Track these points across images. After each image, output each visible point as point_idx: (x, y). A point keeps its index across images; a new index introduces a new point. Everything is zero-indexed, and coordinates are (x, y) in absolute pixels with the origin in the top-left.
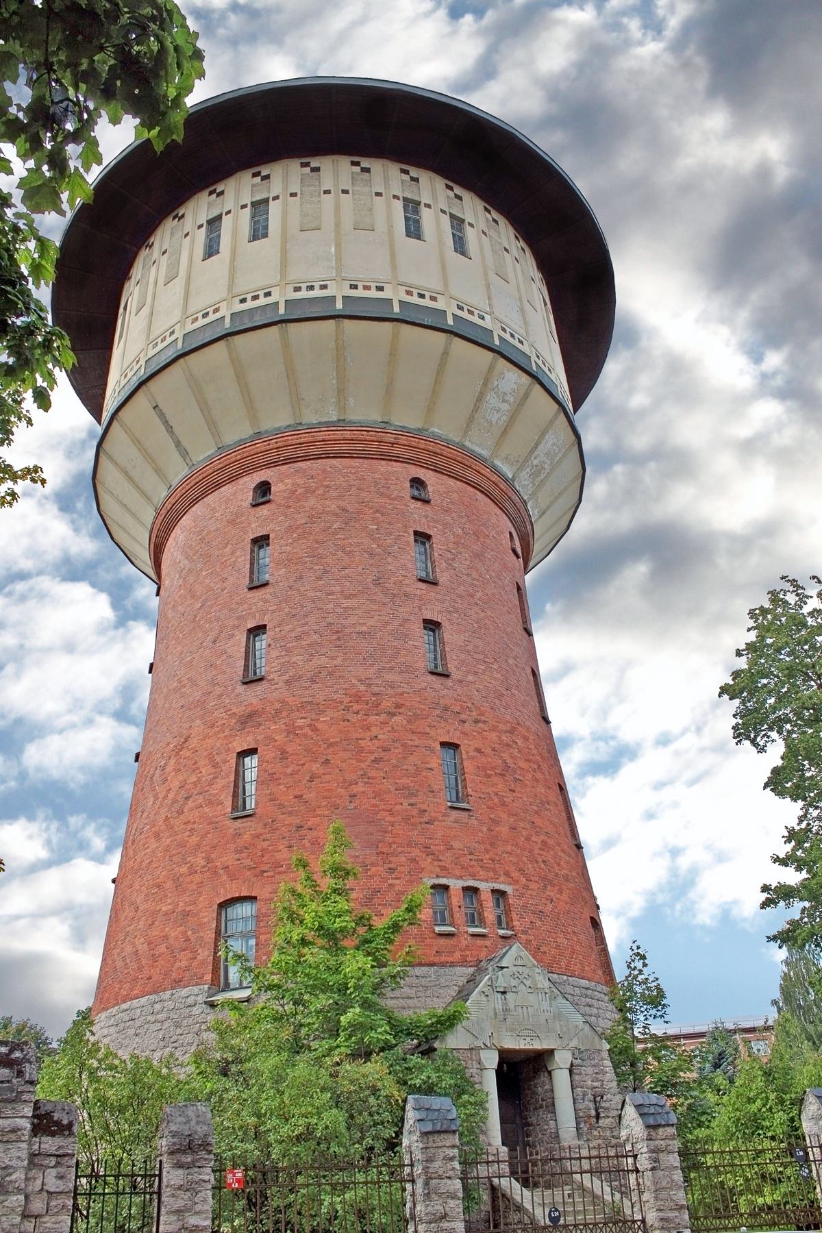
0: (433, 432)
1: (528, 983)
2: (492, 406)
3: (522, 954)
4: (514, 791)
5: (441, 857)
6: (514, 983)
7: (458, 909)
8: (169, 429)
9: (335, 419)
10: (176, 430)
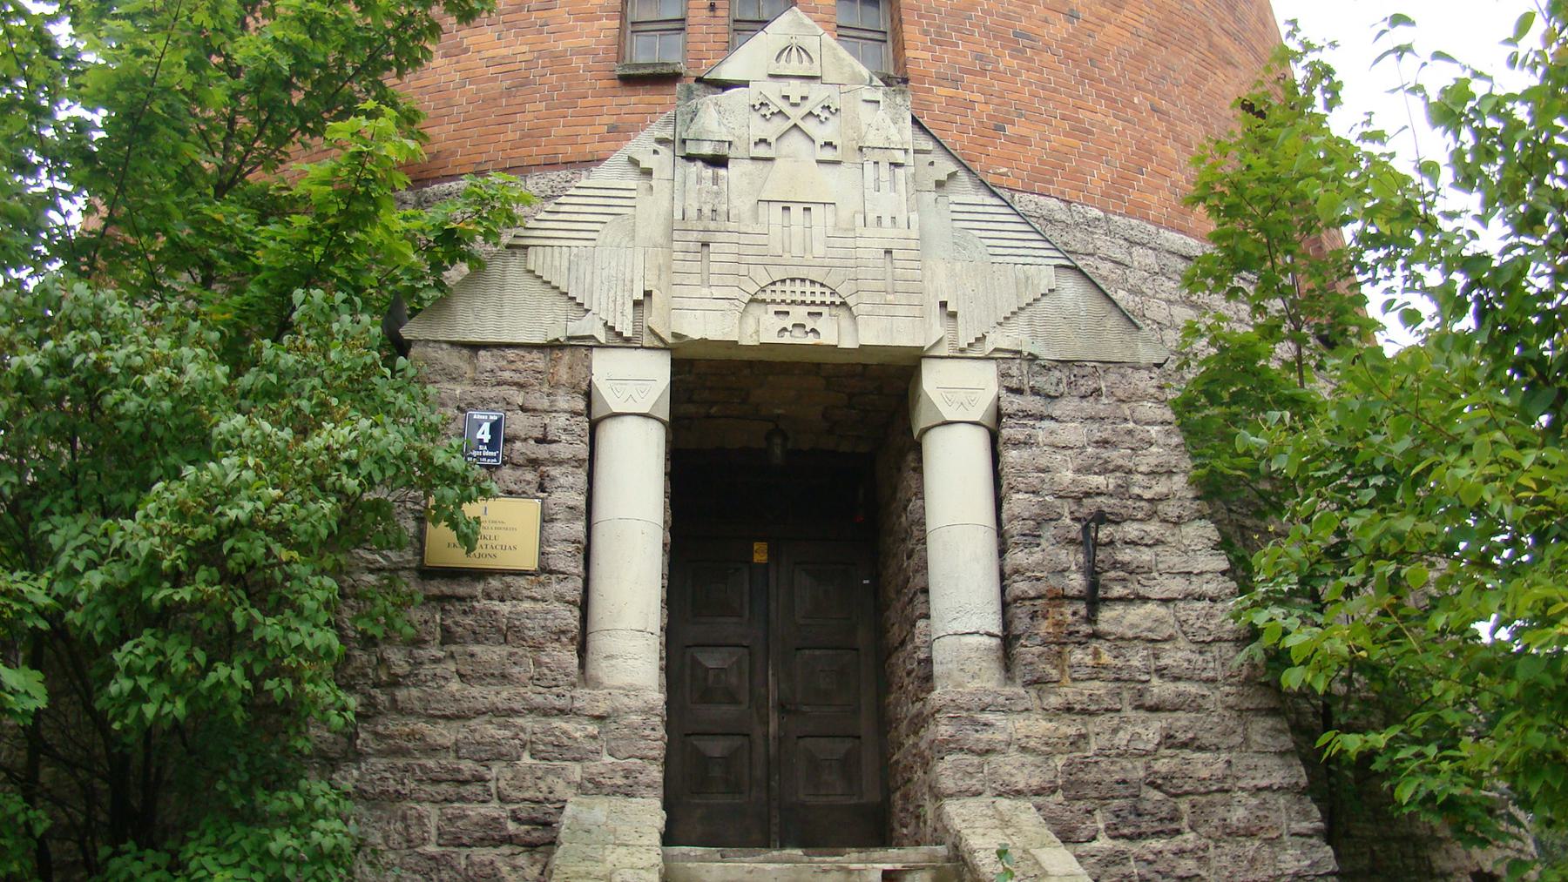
1: (821, 133)
3: (811, 44)
6: (759, 128)
7: (706, 13)
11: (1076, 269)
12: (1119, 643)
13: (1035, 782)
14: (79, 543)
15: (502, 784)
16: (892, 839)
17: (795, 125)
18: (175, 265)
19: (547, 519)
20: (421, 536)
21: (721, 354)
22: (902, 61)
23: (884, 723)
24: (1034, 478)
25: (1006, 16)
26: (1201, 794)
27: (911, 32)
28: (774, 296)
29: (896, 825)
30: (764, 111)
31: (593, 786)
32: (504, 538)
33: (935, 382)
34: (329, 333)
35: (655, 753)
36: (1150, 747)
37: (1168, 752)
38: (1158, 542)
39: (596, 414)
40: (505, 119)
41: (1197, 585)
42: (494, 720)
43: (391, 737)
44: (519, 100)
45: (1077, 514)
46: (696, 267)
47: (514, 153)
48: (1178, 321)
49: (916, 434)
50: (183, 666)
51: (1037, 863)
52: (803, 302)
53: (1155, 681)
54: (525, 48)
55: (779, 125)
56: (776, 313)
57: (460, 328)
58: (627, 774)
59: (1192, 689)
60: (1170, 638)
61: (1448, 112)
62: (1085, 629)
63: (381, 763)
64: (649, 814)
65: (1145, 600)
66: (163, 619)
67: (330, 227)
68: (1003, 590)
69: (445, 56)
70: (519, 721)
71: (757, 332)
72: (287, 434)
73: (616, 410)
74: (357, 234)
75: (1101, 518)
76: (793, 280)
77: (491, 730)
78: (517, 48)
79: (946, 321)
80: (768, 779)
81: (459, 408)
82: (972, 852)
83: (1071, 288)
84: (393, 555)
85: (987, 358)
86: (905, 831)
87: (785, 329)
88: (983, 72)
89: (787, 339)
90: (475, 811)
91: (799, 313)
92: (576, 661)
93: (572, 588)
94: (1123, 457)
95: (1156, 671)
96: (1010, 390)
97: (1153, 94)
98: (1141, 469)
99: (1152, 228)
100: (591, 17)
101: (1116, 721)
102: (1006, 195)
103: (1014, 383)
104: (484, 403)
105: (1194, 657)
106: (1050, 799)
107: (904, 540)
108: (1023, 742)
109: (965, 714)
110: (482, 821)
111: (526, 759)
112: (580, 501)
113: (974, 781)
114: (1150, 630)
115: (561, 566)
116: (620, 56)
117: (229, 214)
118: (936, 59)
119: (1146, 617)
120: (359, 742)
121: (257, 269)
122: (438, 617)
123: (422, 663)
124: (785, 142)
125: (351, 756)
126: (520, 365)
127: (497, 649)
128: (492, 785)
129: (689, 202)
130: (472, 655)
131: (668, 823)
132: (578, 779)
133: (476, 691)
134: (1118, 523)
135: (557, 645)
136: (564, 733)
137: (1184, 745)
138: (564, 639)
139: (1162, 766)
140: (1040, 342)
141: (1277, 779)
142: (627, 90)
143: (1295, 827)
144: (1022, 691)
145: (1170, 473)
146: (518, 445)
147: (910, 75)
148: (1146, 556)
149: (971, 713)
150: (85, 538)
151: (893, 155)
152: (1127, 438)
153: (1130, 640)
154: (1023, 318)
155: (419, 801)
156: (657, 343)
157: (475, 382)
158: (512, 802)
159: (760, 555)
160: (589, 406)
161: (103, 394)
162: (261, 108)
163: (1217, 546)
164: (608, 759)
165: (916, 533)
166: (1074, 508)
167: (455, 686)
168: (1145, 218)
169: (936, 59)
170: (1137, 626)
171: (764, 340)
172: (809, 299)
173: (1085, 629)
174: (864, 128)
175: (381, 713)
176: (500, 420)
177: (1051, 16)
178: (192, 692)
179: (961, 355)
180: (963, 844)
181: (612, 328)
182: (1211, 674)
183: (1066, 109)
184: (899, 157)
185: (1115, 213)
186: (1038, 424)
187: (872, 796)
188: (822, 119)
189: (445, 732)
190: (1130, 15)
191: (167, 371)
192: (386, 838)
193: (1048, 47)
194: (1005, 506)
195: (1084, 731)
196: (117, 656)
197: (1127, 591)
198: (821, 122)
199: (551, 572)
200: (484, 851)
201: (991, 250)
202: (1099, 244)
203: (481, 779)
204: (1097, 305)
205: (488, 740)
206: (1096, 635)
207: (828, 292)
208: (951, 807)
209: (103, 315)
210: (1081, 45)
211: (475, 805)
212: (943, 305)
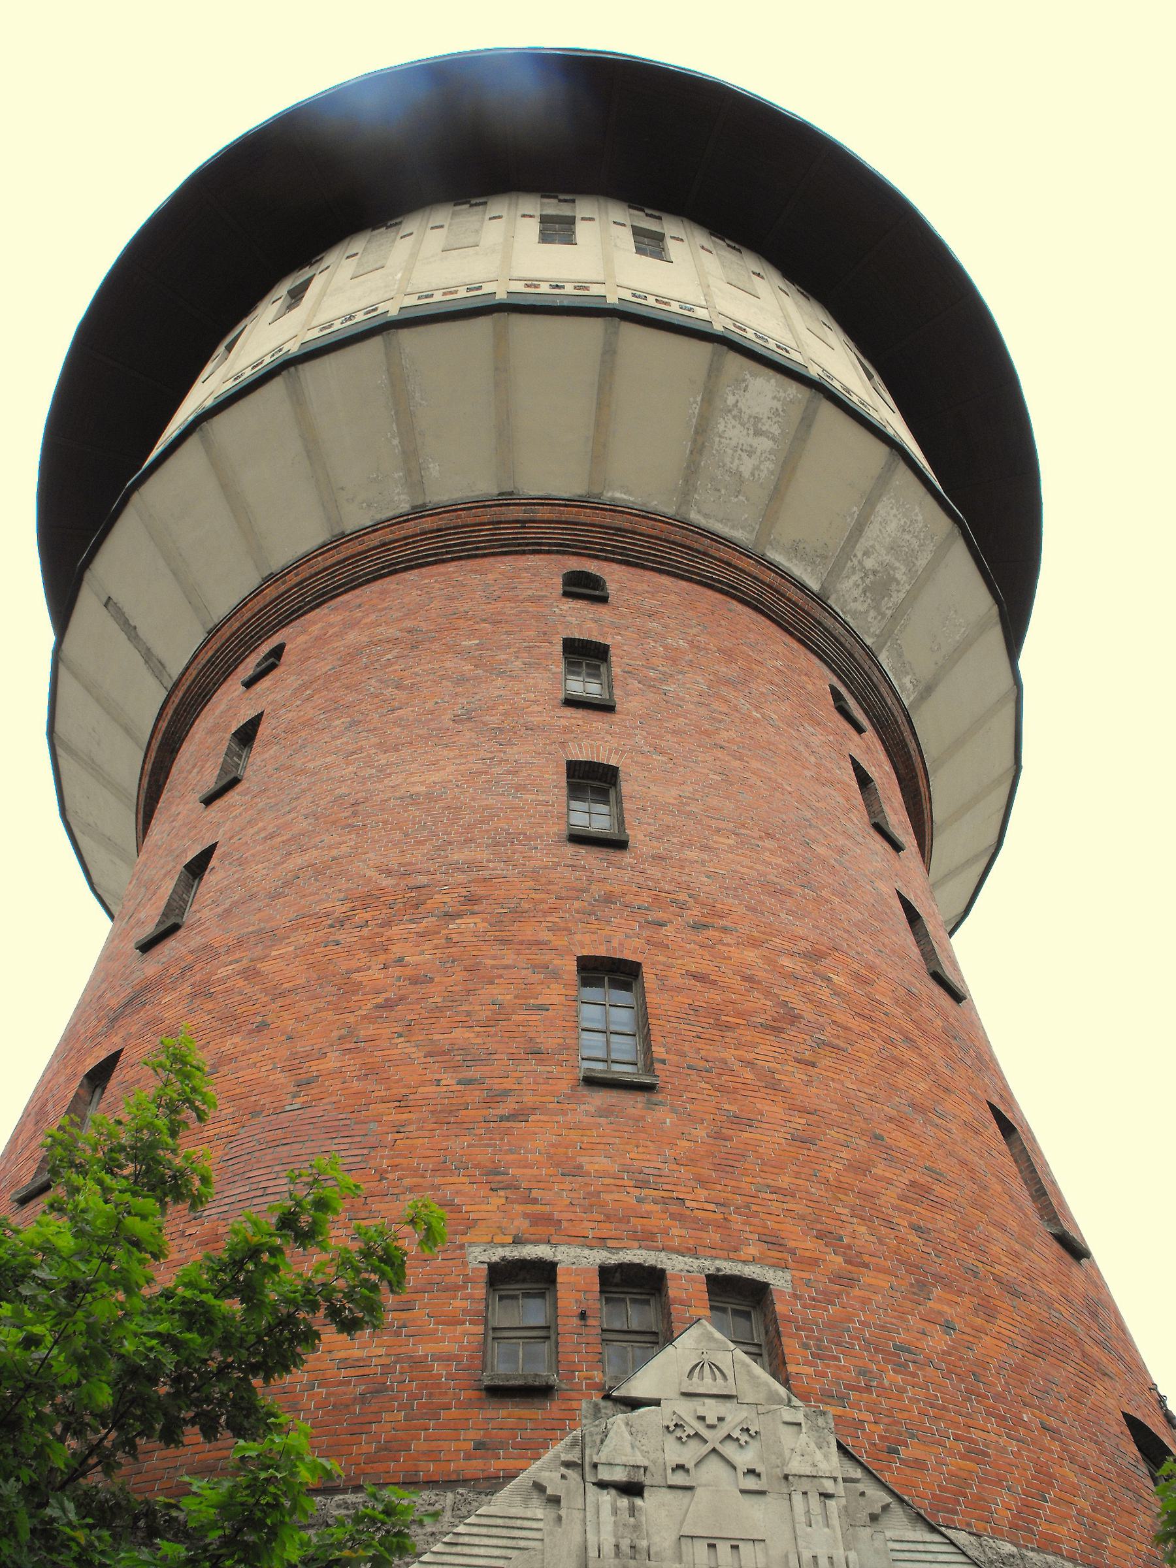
0: (613, 499)
1: (744, 1458)
2: (734, 443)
3: (723, 1360)
4: (814, 1065)
5: (535, 1194)
6: (674, 1453)
7: (575, 1321)
8: (130, 631)
9: (405, 507)
10: (143, 631)
17: (714, 1450)
25: (883, 1328)
27: (790, 1345)
30: (679, 1433)
54: (382, 1351)
61: (384, 1249)
88: (868, 1388)
100: (454, 1321)
118: (821, 1375)
129: (604, 1536)
151: (822, 1485)
168: (1058, 1553)
169: (821, 1375)
174: (787, 1453)
177: (929, 1327)
183: (958, 1428)
184: (829, 1487)
188: (742, 1442)
190: (1003, 1325)
198: (741, 1446)
210: (961, 1358)
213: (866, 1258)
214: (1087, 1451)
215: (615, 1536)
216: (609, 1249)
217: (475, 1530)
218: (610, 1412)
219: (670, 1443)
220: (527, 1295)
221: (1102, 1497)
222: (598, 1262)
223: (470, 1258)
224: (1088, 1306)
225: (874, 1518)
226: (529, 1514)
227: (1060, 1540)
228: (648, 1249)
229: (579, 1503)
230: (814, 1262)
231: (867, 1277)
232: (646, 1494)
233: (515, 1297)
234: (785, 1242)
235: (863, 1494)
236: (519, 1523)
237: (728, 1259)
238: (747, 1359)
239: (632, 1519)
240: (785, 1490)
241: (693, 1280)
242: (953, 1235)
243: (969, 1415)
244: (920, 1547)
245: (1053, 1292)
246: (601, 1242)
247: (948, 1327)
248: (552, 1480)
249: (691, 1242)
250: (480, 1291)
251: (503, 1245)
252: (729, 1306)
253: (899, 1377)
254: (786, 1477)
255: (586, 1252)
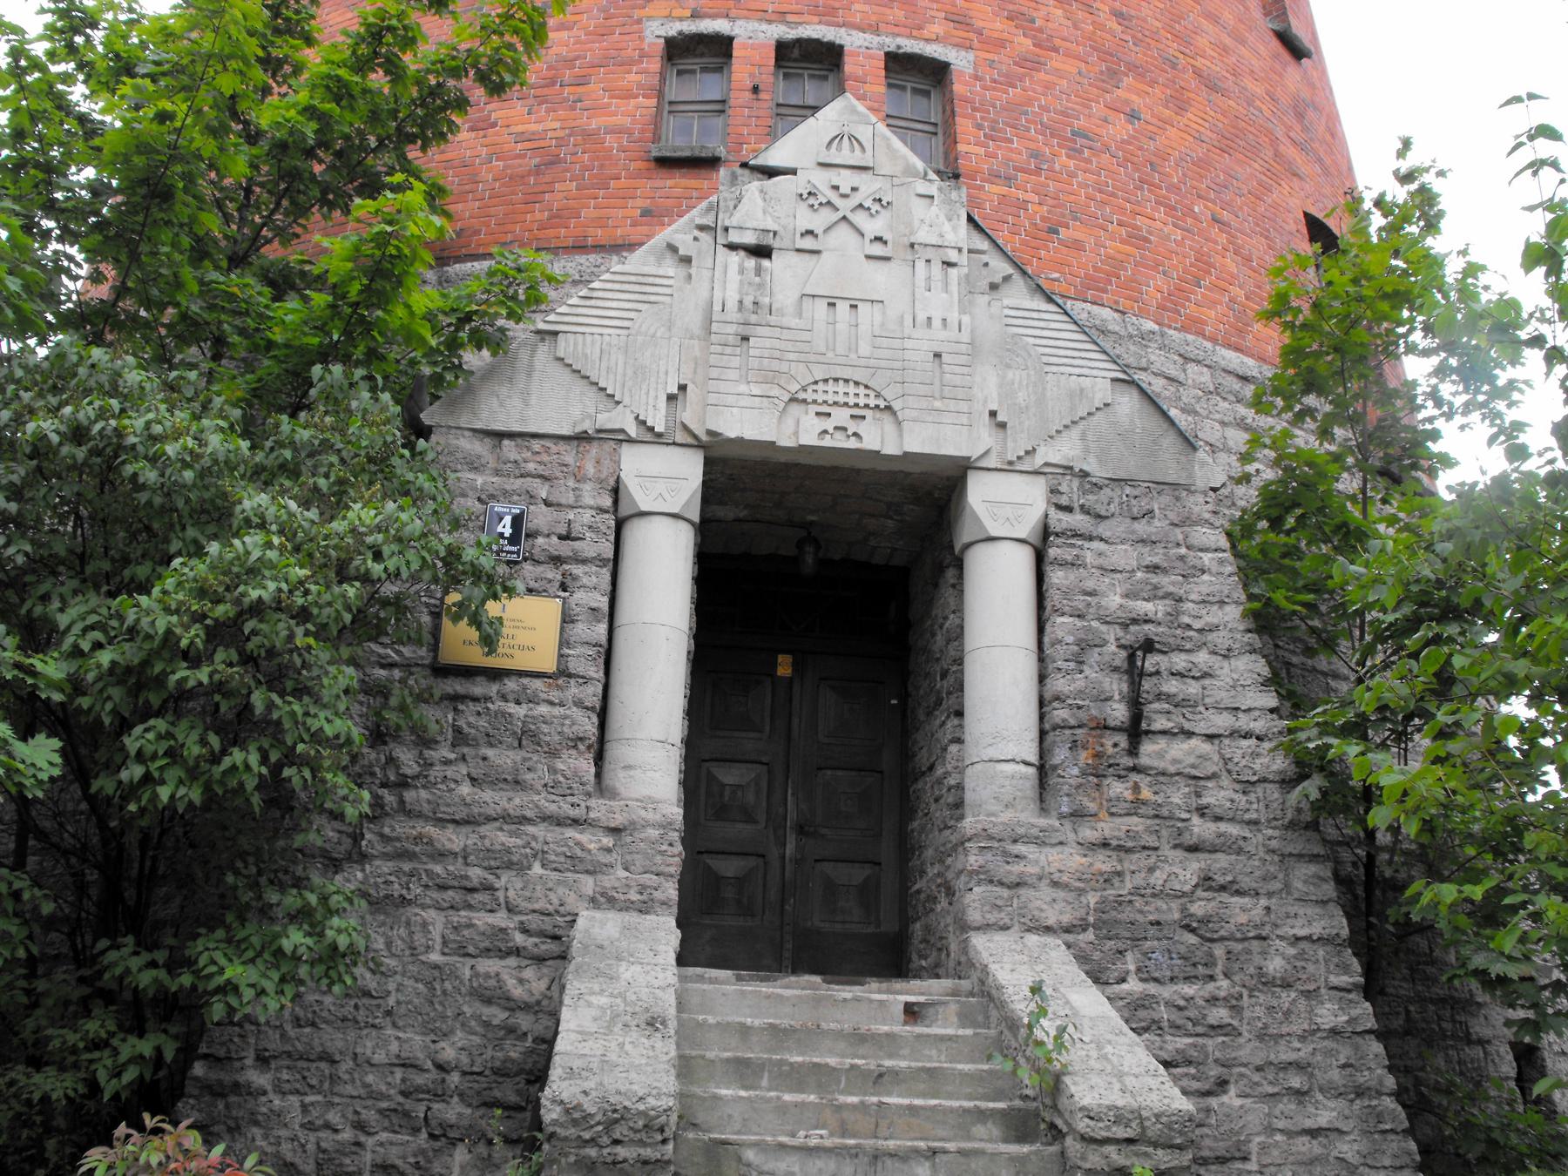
1: (872, 227)
3: (864, 133)
6: (806, 219)
7: (748, 95)
11: (1132, 383)
12: (1161, 779)
13: (1066, 919)
14: (88, 622)
15: (511, 893)
16: (908, 970)
17: (844, 218)
18: (183, 340)
19: (567, 619)
20: (436, 632)
21: (755, 454)
22: (952, 157)
23: (906, 849)
24: (1079, 601)
26: (1237, 940)
27: (963, 125)
28: (815, 396)
29: (914, 957)
30: (811, 201)
31: (605, 900)
32: (523, 638)
33: (981, 494)
34: (349, 412)
35: (672, 870)
36: (1187, 888)
37: (1206, 894)
38: (1206, 675)
39: (624, 511)
40: (533, 199)
41: (1244, 723)
42: (506, 827)
43: (398, 839)
44: (547, 179)
45: (1123, 641)
46: (736, 361)
47: (541, 234)
48: (1231, 443)
49: (957, 550)
50: (196, 750)
51: (1067, 1002)
52: (846, 404)
53: (1196, 820)
54: (557, 125)
55: (827, 216)
56: (818, 414)
57: (484, 415)
58: (642, 889)
59: (1233, 830)
60: (1214, 776)
62: (1128, 761)
63: (386, 867)
64: (665, 933)
65: (1190, 734)
66: (177, 703)
67: (351, 305)
68: (1042, 717)
69: (472, 129)
70: (531, 829)
71: (796, 433)
72: (313, 514)
73: (644, 508)
74: (380, 313)
75: (1148, 646)
76: (836, 380)
77: (502, 837)
78: (548, 124)
79: (994, 430)
80: (783, 902)
81: (479, 499)
82: (999, 988)
83: (1128, 403)
84: (407, 651)
85: (1036, 473)
86: (924, 963)
87: (825, 432)
89: (827, 442)
90: (482, 920)
91: (841, 416)
92: (593, 770)
93: (592, 693)
94: (1173, 584)
95: (1197, 809)
96: (1059, 507)
97: (1214, 202)
98: (1193, 597)
99: (1208, 345)
101: (1153, 860)
102: (1060, 301)
103: (1064, 501)
104: (506, 495)
105: (1236, 797)
106: (1081, 937)
107: (938, 660)
108: (1056, 877)
109: (996, 844)
110: (489, 932)
111: (537, 869)
112: (602, 603)
113: (1003, 915)
114: (1193, 766)
115: (581, 670)
116: (656, 139)
117: (247, 286)
119: (1190, 752)
120: (364, 843)
121: (270, 345)
122: (450, 717)
123: (431, 765)
124: (834, 233)
125: (355, 857)
126: (545, 458)
127: (510, 753)
128: (500, 894)
130: (484, 759)
131: (683, 941)
132: (590, 893)
133: (487, 795)
134: (1165, 653)
135: (573, 752)
136: (578, 843)
137: (1223, 888)
138: (581, 747)
139: (1198, 909)
140: (1092, 459)
141: (1316, 929)
142: (663, 172)
143: (1335, 980)
144: (1057, 824)
145: (1222, 603)
146: (540, 540)
147: (962, 171)
148: (1193, 688)
149: (1004, 841)
150: (93, 619)
152: (1179, 564)
153: (1172, 775)
154: (1075, 433)
155: (424, 907)
156: (690, 440)
157: (497, 472)
158: (520, 913)
159: (784, 667)
160: (616, 502)
161: (124, 462)
162: (281, 178)
163: (1266, 683)
164: (623, 874)
165: (952, 653)
166: (1121, 633)
167: (465, 789)
168: (1201, 334)
170: (1179, 762)
171: (802, 442)
172: (852, 401)
173: (1128, 761)
174: (916, 223)
175: (387, 814)
176: (522, 513)
177: (1111, 116)
178: (206, 777)
179: (1009, 468)
180: (991, 978)
181: (644, 423)
182: (1254, 816)
184: (953, 256)
185: (1170, 327)
186: (1087, 544)
187: (889, 925)
189: (454, 837)
191: (190, 442)
192: (389, 944)
193: (1107, 148)
194: (1048, 628)
195: (1119, 868)
196: (127, 740)
197: (1171, 725)
199: (570, 676)
200: (490, 962)
201: (1045, 359)
202: (1153, 358)
203: (490, 888)
204: (1154, 423)
205: (498, 847)
206: (1135, 769)
207: (872, 394)
208: (979, 941)
209: (121, 382)
210: (1141, 149)
211: (482, 914)
212: (993, 414)
213: (1057, 42)
214: (1255, 246)
215: (740, 292)
216: (788, 23)
217: (609, 286)
218: (746, 179)
219: (802, 209)
220: (704, 70)
221: (1259, 287)
222: (776, 36)
223: (648, 33)
224: (1295, 108)
225: (994, 287)
226: (661, 272)
227: (1204, 323)
228: (829, 24)
229: (709, 264)
230: (1000, 44)
231: (1055, 62)
232: (774, 256)
233: (693, 72)
234: (974, 21)
235: (986, 265)
236: (651, 280)
237: (910, 36)
238: (887, 132)
239: (757, 279)
240: (910, 258)
241: (872, 57)
242: (1159, 25)
243: (1138, 203)
244: (1035, 315)
245: (1258, 89)
246: (781, 16)
247: (1133, 116)
248: (686, 246)
249: (874, 18)
250: (655, 65)
251: (681, 19)
252: (909, 85)
253: (1072, 163)
254: (912, 245)
255: (764, 27)
